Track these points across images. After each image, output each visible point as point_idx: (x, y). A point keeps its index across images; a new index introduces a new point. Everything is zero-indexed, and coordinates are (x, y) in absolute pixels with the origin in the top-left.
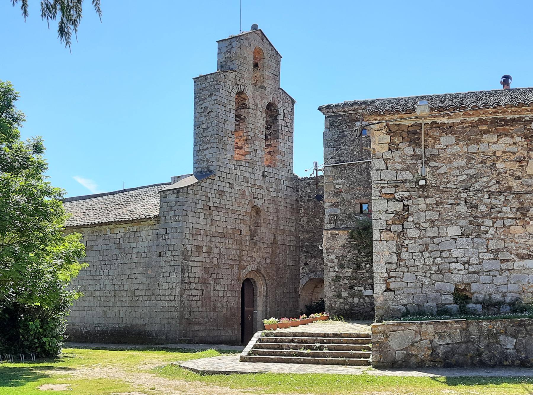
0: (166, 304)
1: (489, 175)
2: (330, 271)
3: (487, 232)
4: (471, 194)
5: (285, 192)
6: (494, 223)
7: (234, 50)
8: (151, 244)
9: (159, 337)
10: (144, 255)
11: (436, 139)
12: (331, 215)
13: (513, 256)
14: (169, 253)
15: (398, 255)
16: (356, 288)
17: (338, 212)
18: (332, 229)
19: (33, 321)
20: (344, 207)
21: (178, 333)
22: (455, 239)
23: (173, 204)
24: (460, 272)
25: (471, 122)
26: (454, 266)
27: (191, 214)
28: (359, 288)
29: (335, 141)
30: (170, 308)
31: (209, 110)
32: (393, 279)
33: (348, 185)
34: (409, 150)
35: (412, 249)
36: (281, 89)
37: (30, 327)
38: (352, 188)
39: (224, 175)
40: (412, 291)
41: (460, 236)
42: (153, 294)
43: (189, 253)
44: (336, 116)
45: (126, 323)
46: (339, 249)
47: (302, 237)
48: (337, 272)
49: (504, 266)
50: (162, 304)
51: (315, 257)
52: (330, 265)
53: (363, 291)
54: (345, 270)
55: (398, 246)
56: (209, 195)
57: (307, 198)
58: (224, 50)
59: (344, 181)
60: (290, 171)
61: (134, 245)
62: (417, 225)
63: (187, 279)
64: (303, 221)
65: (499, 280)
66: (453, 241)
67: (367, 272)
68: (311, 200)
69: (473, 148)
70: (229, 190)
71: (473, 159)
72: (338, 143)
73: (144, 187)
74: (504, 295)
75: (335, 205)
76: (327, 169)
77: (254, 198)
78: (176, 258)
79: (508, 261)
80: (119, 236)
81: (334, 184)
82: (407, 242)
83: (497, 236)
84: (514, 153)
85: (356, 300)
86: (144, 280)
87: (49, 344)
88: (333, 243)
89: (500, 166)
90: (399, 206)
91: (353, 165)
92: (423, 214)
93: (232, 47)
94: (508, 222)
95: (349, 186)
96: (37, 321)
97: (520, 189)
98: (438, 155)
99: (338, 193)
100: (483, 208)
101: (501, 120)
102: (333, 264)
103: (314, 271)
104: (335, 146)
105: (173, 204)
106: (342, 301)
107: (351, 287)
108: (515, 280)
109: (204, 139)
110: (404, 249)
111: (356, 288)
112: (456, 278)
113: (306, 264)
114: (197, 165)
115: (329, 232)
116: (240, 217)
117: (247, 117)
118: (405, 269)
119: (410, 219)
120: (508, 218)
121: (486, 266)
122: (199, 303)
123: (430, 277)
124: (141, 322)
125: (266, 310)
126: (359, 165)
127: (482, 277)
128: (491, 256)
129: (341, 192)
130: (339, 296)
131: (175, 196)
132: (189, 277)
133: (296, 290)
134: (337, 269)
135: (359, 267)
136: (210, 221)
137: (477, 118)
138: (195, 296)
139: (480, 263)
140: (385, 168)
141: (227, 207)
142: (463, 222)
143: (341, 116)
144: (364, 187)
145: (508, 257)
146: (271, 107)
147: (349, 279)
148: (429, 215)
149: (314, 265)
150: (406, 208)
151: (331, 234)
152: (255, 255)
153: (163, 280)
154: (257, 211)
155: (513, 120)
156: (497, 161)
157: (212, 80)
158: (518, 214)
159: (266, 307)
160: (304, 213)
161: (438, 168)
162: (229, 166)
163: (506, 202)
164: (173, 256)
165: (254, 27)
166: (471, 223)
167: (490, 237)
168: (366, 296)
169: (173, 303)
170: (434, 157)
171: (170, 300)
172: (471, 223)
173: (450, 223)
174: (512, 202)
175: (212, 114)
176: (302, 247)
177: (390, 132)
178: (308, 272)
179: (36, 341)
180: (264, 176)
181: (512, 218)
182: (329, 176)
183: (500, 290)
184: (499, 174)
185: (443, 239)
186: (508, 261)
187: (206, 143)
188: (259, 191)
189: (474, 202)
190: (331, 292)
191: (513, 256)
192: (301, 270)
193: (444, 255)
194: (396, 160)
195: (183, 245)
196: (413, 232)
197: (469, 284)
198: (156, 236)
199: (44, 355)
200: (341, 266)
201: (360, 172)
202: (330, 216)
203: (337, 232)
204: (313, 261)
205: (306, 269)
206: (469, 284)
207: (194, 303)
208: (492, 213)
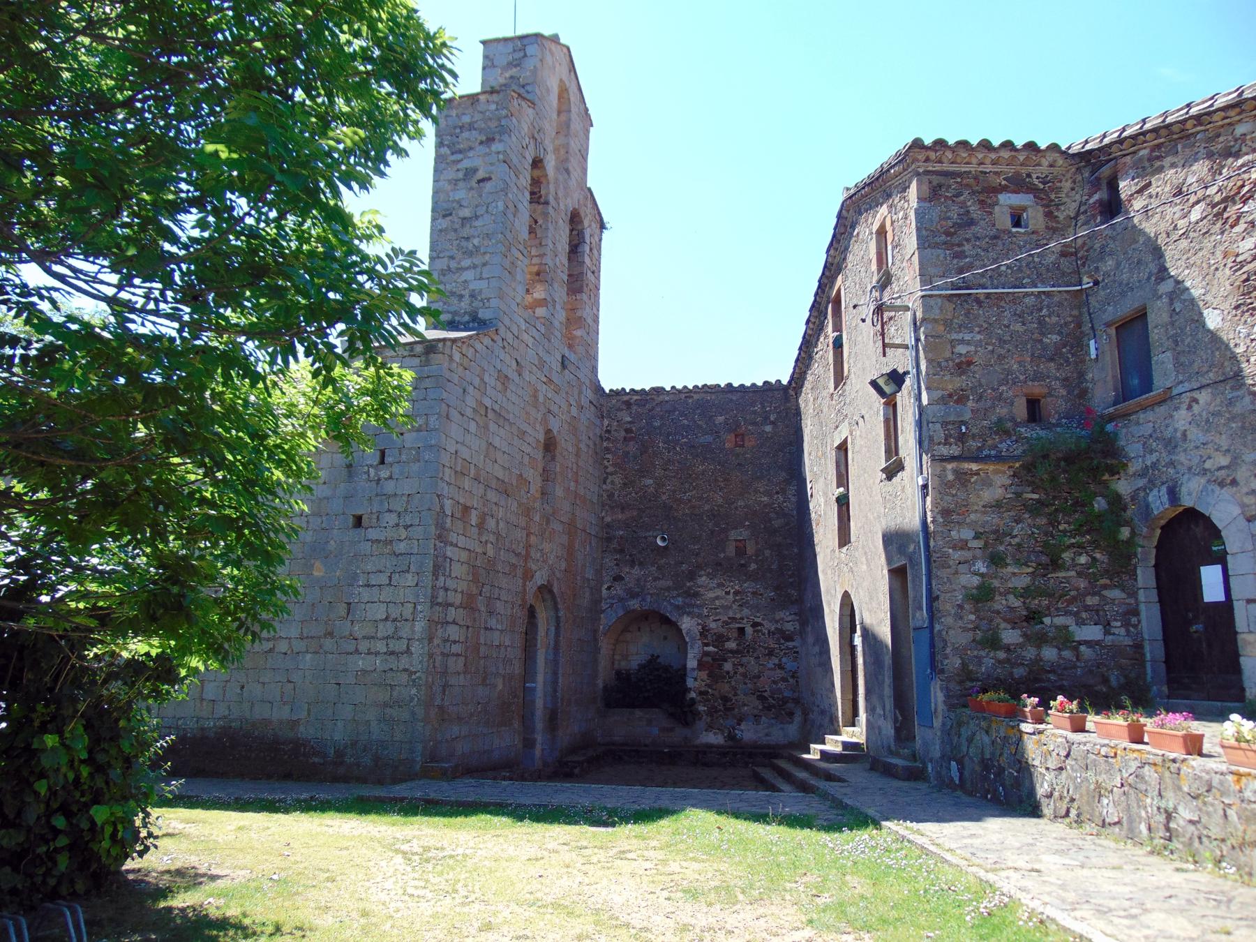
2: (956, 573)
9: (348, 760)
12: (949, 423)
14: (392, 519)
16: (1047, 620)
17: (967, 416)
18: (953, 458)
19: (60, 732)
20: (981, 405)
21: (419, 747)
27: (454, 414)
28: (1059, 621)
29: (948, 234)
30: (389, 675)
31: (481, 174)
33: (990, 348)
36: (589, 190)
37: (46, 762)
38: (1001, 358)
42: (330, 634)
43: (449, 520)
45: (225, 717)
46: (984, 513)
47: (608, 519)
48: (982, 575)
51: (641, 564)
52: (957, 555)
53: (1073, 628)
54: (1010, 569)
56: (486, 378)
57: (623, 434)
58: (502, 61)
59: (978, 337)
63: (442, 593)
64: (612, 483)
67: (1079, 574)
68: (632, 439)
70: (516, 378)
72: (956, 240)
76: (932, 302)
78: (417, 532)
81: (953, 343)
85: (1049, 653)
87: (114, 836)
88: (961, 495)
91: (1000, 297)
93: (525, 55)
95: (993, 351)
96: (75, 727)
102: (967, 555)
106: (1001, 655)
107: (1033, 617)
109: (464, 243)
111: (1047, 620)
113: (618, 578)
115: (949, 466)
117: (540, 222)
124: (281, 714)
125: (555, 682)
126: (1015, 299)
129: (970, 363)
130: (993, 642)
132: (446, 590)
134: (981, 567)
135: (1056, 564)
136: (484, 445)
138: (455, 642)
143: (959, 174)
144: (1033, 355)
146: (575, 219)
147: (1026, 593)
149: (638, 580)
151: (955, 471)
152: (546, 546)
153: (366, 595)
157: (493, 107)
159: (555, 673)
160: (614, 465)
164: (406, 527)
169: (404, 662)
171: (392, 653)
175: (488, 186)
179: (60, 822)
182: (935, 321)
188: (557, 399)
190: (965, 630)
192: (604, 591)
195: (438, 496)
198: (344, 472)
199: (80, 887)
200: (996, 560)
203: (974, 467)
204: (636, 571)
205: (619, 590)
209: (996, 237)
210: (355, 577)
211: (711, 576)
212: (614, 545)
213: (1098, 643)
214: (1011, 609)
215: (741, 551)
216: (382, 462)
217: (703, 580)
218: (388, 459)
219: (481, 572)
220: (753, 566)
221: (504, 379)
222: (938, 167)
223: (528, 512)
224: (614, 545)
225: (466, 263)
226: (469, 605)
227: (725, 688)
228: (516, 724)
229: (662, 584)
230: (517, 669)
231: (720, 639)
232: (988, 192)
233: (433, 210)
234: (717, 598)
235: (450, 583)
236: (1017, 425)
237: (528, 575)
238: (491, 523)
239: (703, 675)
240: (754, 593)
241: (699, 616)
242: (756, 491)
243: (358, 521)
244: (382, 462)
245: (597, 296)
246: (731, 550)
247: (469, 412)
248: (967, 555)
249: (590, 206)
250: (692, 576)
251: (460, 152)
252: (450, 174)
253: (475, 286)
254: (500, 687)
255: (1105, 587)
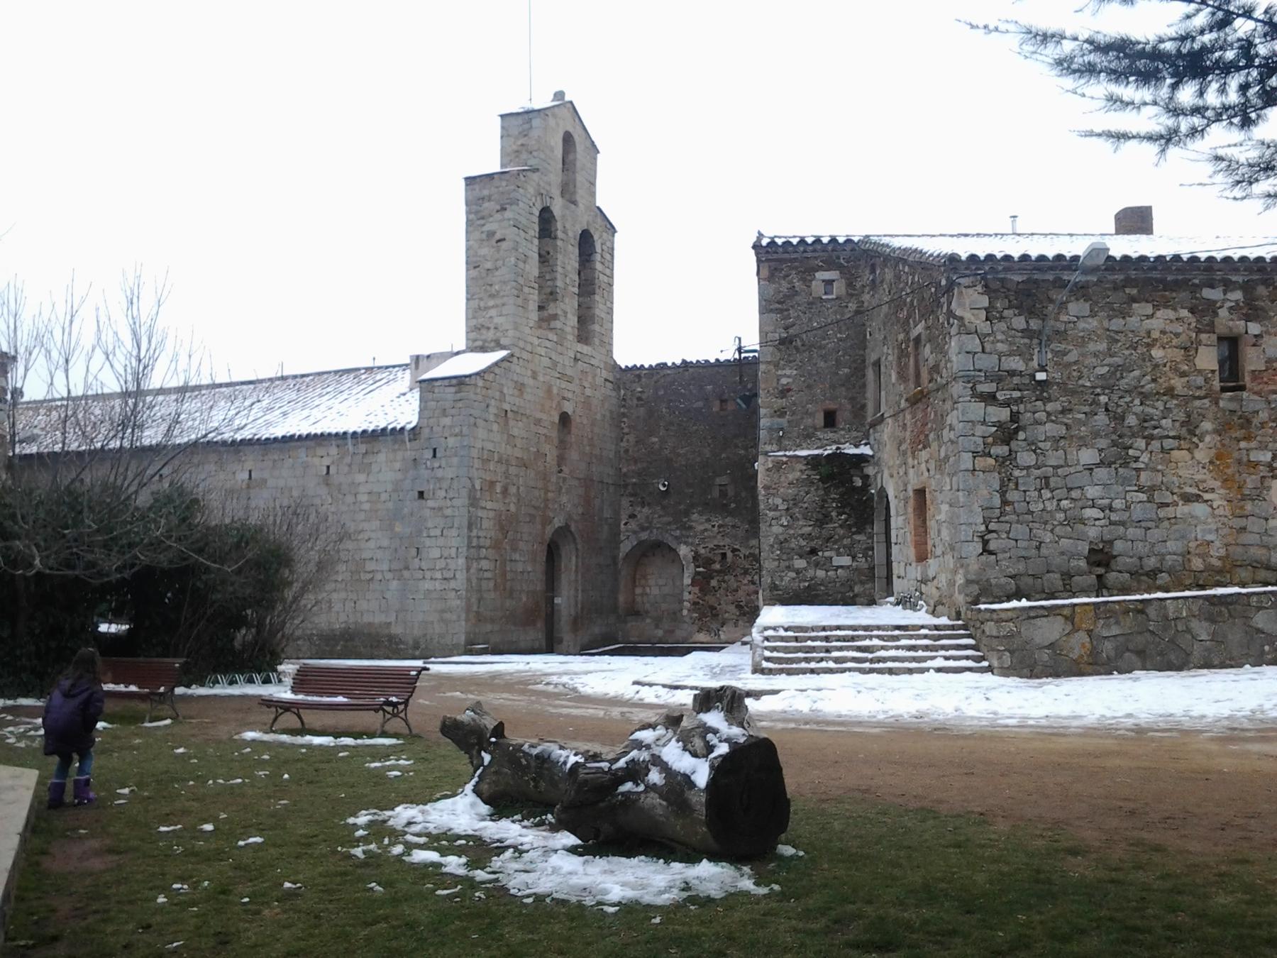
0: (438, 585)
1: (1141, 367)
3: (1137, 459)
4: (1115, 398)
5: (603, 390)
6: (1147, 444)
7: (535, 134)
8: (399, 476)
10: (384, 497)
11: (1063, 306)
13: (1175, 497)
15: (1003, 494)
20: (794, 417)
22: (1091, 469)
23: (448, 405)
24: (1097, 523)
25: (1114, 282)
26: (1090, 513)
27: (480, 422)
28: (827, 554)
29: (779, 303)
31: (498, 236)
32: (994, 535)
34: (1019, 322)
35: (1024, 484)
36: (598, 208)
39: (525, 355)
40: (1024, 553)
41: (1098, 466)
42: (407, 568)
44: (780, 261)
47: (624, 470)
49: (1162, 513)
50: (427, 585)
51: (649, 504)
52: (771, 514)
55: (1002, 480)
56: (505, 391)
57: (635, 401)
58: (515, 132)
60: (610, 352)
61: (361, 478)
62: (1033, 446)
65: (1155, 534)
66: (1087, 472)
68: (642, 406)
69: (1117, 324)
70: (531, 382)
71: (1118, 341)
73: (308, 375)
74: (1162, 557)
75: (781, 413)
77: (564, 398)
78: (456, 502)
79: (1167, 505)
80: (326, 461)
82: (1017, 473)
83: (1151, 465)
84: (1177, 335)
85: (821, 574)
86: (385, 543)
89: (1157, 353)
90: (1004, 414)
92: (1041, 428)
94: (1168, 443)
97: (1186, 391)
98: (1066, 331)
99: (784, 392)
100: (1132, 420)
101: (1157, 280)
102: (778, 514)
103: (647, 528)
104: (780, 311)
105: (448, 405)
108: (1177, 535)
110: (1012, 485)
112: (1093, 532)
113: (632, 516)
114: (473, 335)
116: (545, 431)
118: (1014, 517)
119: (1021, 435)
120: (1168, 437)
121: (1137, 512)
122: (491, 584)
123: (1052, 531)
127: (1131, 530)
128: (1143, 497)
131: (453, 390)
132: (478, 537)
133: (615, 558)
137: (1122, 277)
139: (1128, 508)
140: (980, 349)
141: (528, 412)
142: (1103, 443)
145: (1169, 498)
146: (586, 240)
148: (1051, 429)
150: (1015, 417)
152: (564, 499)
153: (428, 542)
154: (565, 419)
155: (1176, 282)
156: (1153, 346)
158: (1184, 431)
160: (629, 427)
161: (1065, 353)
162: (530, 339)
163: (1167, 412)
165: (559, 95)
166: (1114, 444)
167: (1142, 466)
168: (838, 567)
170: (1061, 335)
172: (1114, 444)
173: (1083, 443)
174: (1175, 411)
175: (504, 245)
176: (626, 486)
177: (988, 290)
178: (637, 529)
180: (576, 359)
181: (1174, 438)
183: (1156, 549)
184: (1156, 366)
185: (1072, 470)
186: (1167, 505)
187: (492, 296)
188: (570, 386)
189: (1119, 410)
191: (1175, 497)
193: (1074, 494)
194: (999, 337)
196: (1026, 458)
197: (1111, 542)
201: (824, 358)
202: (770, 429)
204: (646, 510)
205: (633, 525)
206: (1111, 542)
207: (484, 584)
208: (1146, 428)
209: (812, 303)
210: (420, 531)
211: (701, 513)
212: (630, 489)
213: (848, 567)
214: (801, 547)
215: (723, 494)
216: (434, 456)
217: (695, 517)
218: (438, 455)
219: (505, 524)
220: (733, 505)
221: (521, 387)
222: (775, 256)
223: (545, 477)
224: (630, 489)
225: (491, 303)
226: (496, 545)
227: (711, 600)
228: (540, 624)
229: (666, 519)
230: (540, 587)
231: (708, 562)
232: (807, 273)
233: (467, 263)
234: (706, 530)
235: (481, 534)
236: (816, 429)
237: (547, 521)
238: (513, 490)
239: (696, 590)
240: (733, 526)
241: (692, 544)
242: (736, 446)
243: (421, 494)
244: (434, 456)
245: (611, 293)
246: (716, 493)
247: (492, 418)
248: (778, 514)
249: (599, 220)
250: (687, 513)
251: (483, 218)
252: (477, 235)
253: (498, 320)
254: (524, 599)
255: (854, 533)
